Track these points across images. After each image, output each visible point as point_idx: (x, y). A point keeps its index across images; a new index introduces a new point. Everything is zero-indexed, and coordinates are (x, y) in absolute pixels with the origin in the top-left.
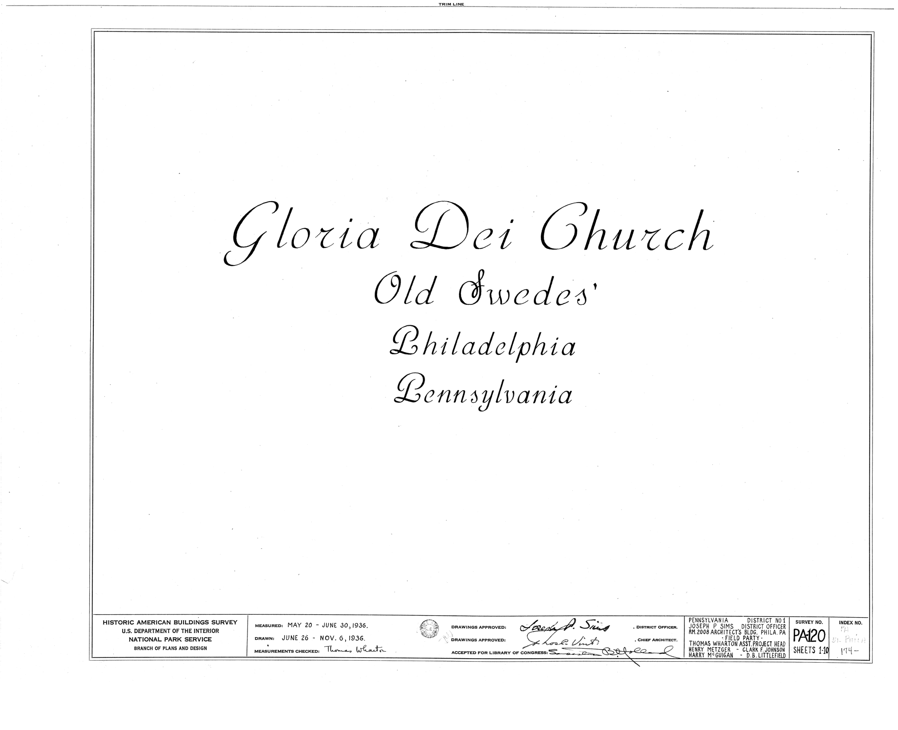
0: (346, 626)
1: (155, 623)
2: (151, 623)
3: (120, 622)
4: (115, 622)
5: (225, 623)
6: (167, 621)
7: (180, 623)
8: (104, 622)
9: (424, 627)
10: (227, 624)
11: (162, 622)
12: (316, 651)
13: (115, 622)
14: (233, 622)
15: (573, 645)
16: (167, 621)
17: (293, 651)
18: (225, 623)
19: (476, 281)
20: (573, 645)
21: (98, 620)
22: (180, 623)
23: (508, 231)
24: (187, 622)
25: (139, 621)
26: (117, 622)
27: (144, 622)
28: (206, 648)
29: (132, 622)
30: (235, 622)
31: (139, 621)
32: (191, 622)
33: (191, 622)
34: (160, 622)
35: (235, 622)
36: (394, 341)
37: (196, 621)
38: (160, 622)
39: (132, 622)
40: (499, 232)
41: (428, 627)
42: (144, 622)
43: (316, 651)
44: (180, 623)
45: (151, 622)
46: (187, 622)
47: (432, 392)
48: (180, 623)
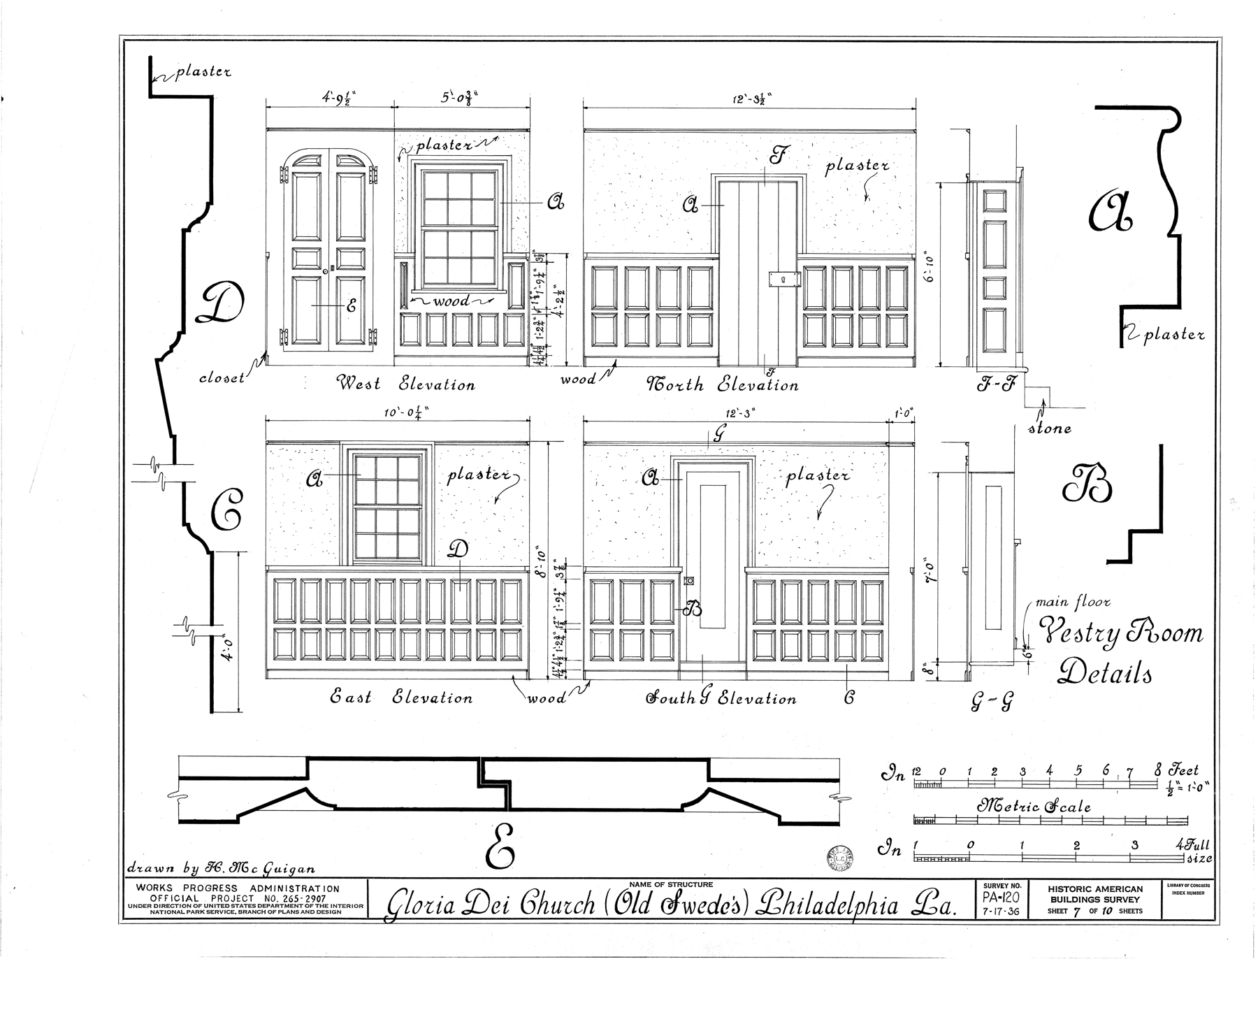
0: (273, 899)
1: (1121, 890)
2: (1115, 890)
3: (1073, 889)
4: (1064, 889)
5: (1122, 900)
6: (1138, 887)
7: (1060, 900)
8: (1050, 889)
9: (833, 856)
10: (1125, 902)
11: (1131, 889)
12: (1174, 893)
13: (1064, 889)
14: (1134, 900)
15: (406, 913)
16: (1138, 887)
17: (1188, 893)
18: (1122, 900)
19: (674, 899)
20: (406, 913)
21: (1206, 774)
22: (1113, 900)
23: (440, 902)
24: (1070, 899)
25: (1098, 887)
26: (1068, 889)
27: (1105, 888)
28: (1203, 893)
29: (1089, 889)
30: (1137, 900)
31: (1098, 887)
32: (1075, 900)
33: (1075, 900)
34: (1128, 889)
35: (1137, 900)
36: (762, 901)
37: (1083, 898)
38: (1128, 889)
39: (1089, 889)
40: (503, 904)
41: (839, 856)
42: (1105, 888)
43: (1174, 893)
44: (1113, 900)
45: (1115, 889)
46: (1070, 899)
47: (419, 904)
48: (1060, 900)
